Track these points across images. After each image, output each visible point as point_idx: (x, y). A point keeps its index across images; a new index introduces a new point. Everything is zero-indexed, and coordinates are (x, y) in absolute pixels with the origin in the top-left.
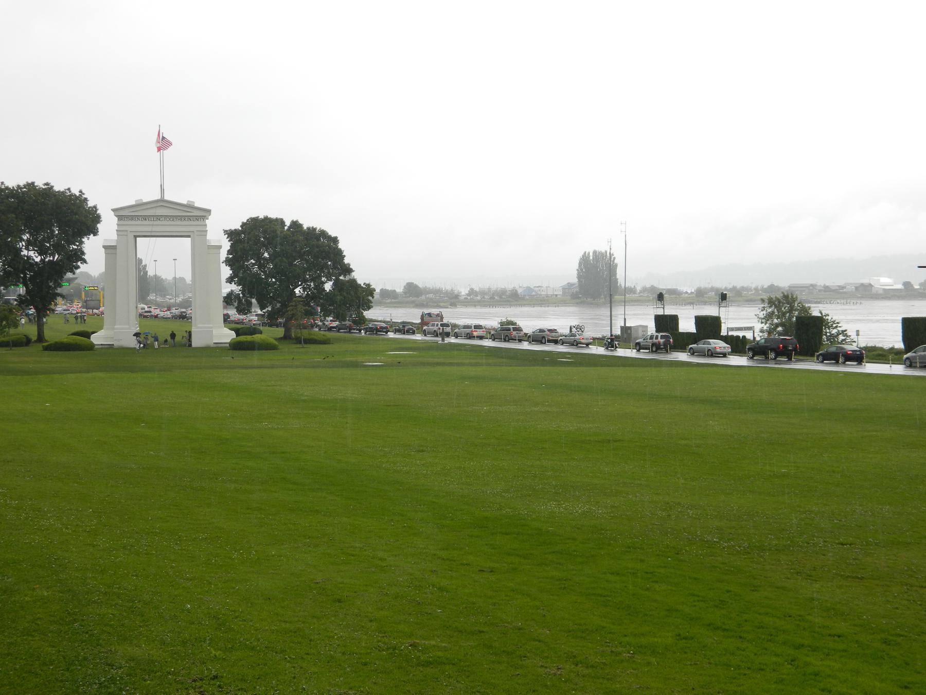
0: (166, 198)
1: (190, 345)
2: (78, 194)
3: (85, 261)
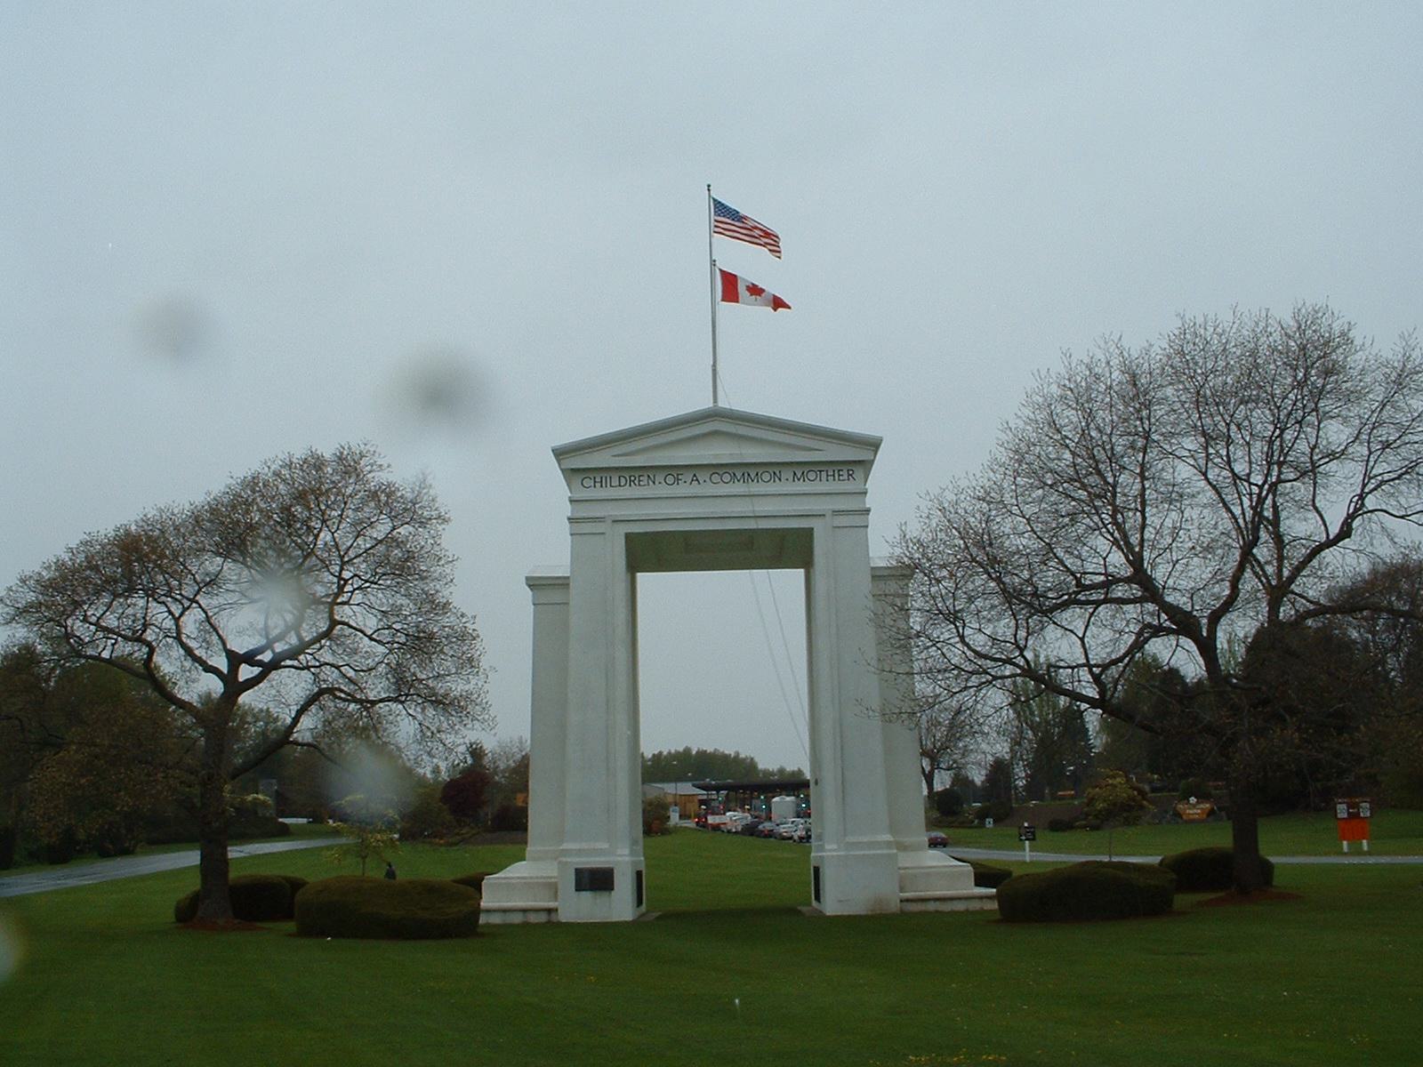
0: (721, 404)
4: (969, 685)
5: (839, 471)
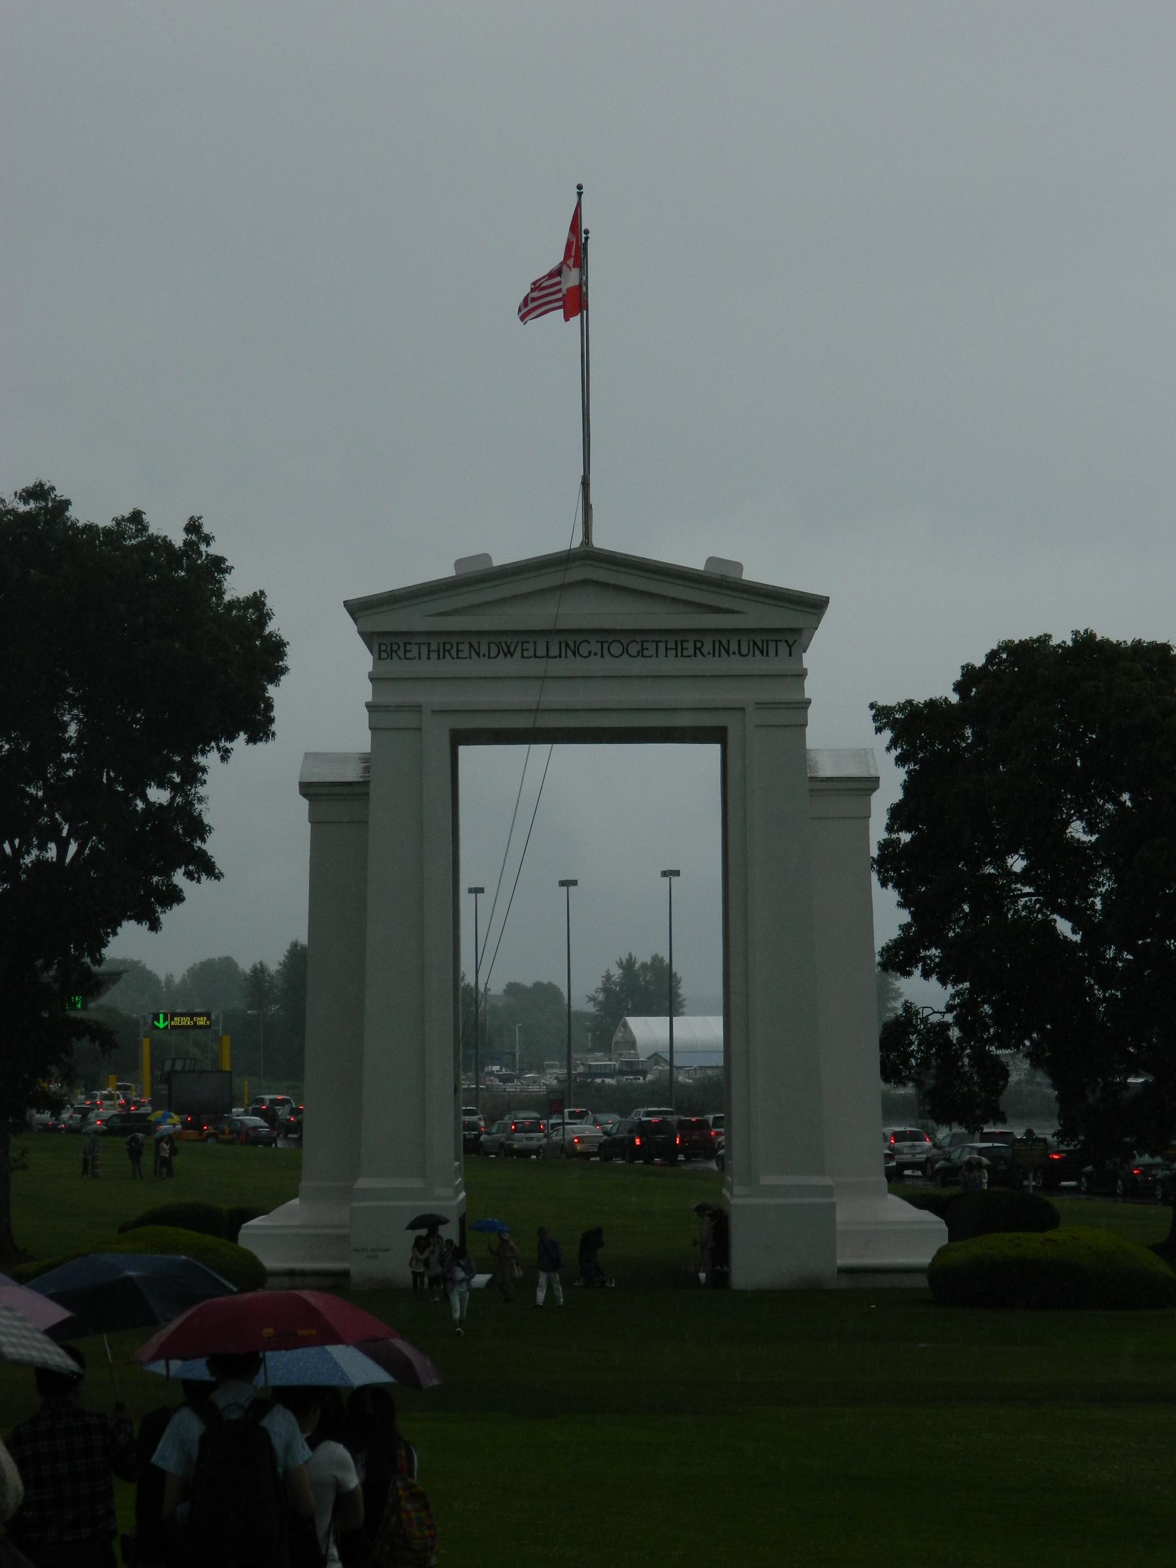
0: (600, 541)
1: (721, 1279)
2: (178, 539)
3: (205, 867)
5: (405, 644)
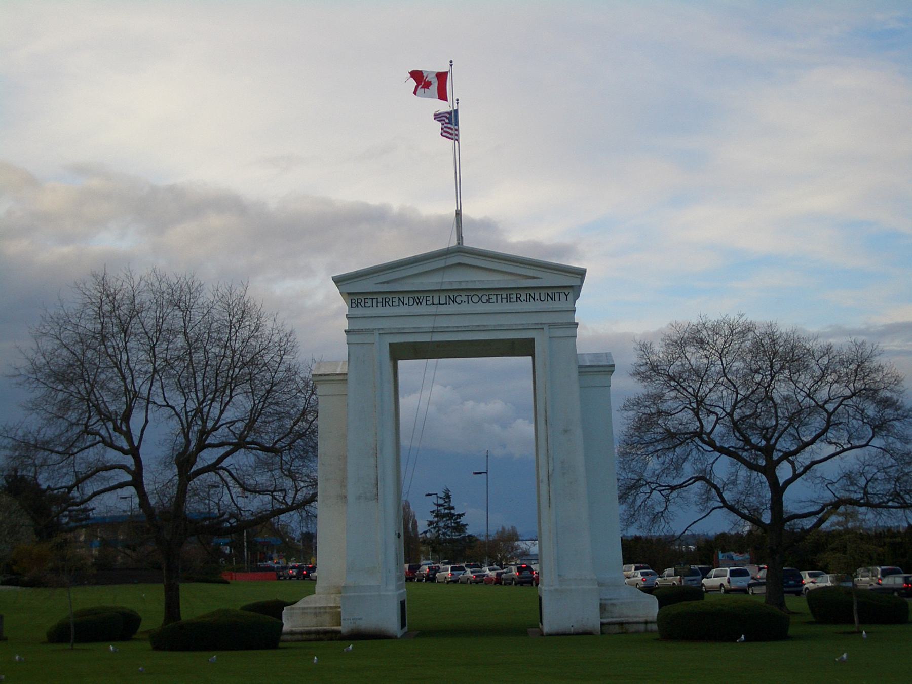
4: (145, 394)
